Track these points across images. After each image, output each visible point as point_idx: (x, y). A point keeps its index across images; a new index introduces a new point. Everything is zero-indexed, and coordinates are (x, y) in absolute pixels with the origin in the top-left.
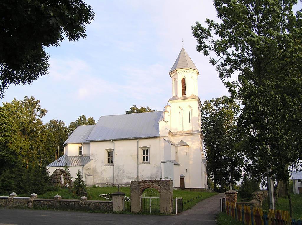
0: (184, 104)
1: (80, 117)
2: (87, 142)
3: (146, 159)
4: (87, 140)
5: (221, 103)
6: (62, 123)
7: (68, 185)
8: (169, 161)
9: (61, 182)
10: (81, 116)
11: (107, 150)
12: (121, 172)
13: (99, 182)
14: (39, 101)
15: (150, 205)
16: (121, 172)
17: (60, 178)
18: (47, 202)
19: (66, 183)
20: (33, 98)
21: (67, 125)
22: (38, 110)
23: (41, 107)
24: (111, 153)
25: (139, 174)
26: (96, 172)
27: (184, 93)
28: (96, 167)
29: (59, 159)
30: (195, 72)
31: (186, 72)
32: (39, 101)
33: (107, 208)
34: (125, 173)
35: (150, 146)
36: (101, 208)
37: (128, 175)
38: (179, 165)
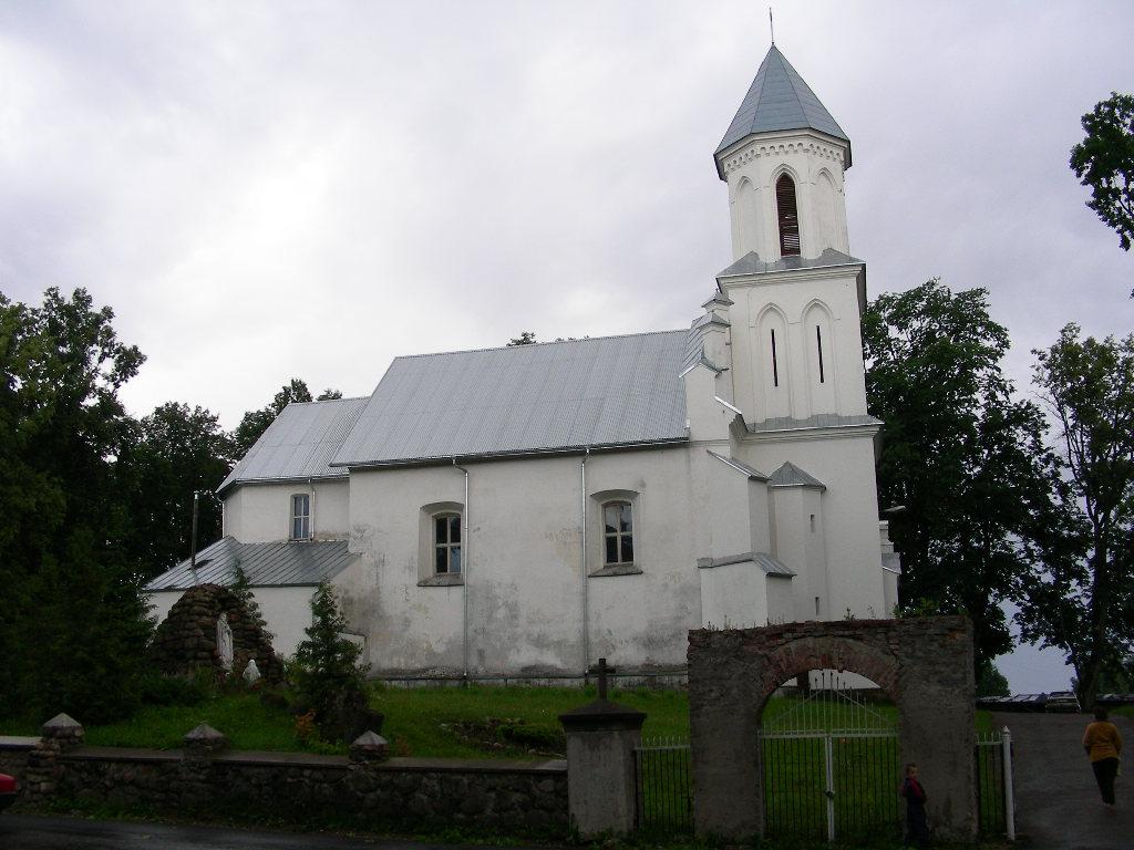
0: (793, 296)
1: (284, 388)
2: (335, 472)
3: (619, 552)
4: (337, 461)
5: (917, 316)
6: (204, 420)
7: (253, 669)
8: (729, 561)
9: (215, 658)
10: (289, 385)
11: (428, 508)
12: (501, 613)
13: (395, 665)
14: (108, 313)
15: (830, 786)
16: (501, 613)
17: (212, 633)
18: (140, 768)
19: (245, 664)
20: (82, 299)
21: (229, 425)
22: (106, 350)
23: (117, 340)
24: (447, 526)
25: (593, 626)
26: (381, 617)
27: (790, 251)
28: (377, 590)
29: (200, 557)
30: (835, 151)
31: (796, 147)
32: (108, 313)
33: (526, 811)
34: (522, 621)
35: (643, 485)
36: (488, 811)
37: (536, 630)
38: (789, 577)
